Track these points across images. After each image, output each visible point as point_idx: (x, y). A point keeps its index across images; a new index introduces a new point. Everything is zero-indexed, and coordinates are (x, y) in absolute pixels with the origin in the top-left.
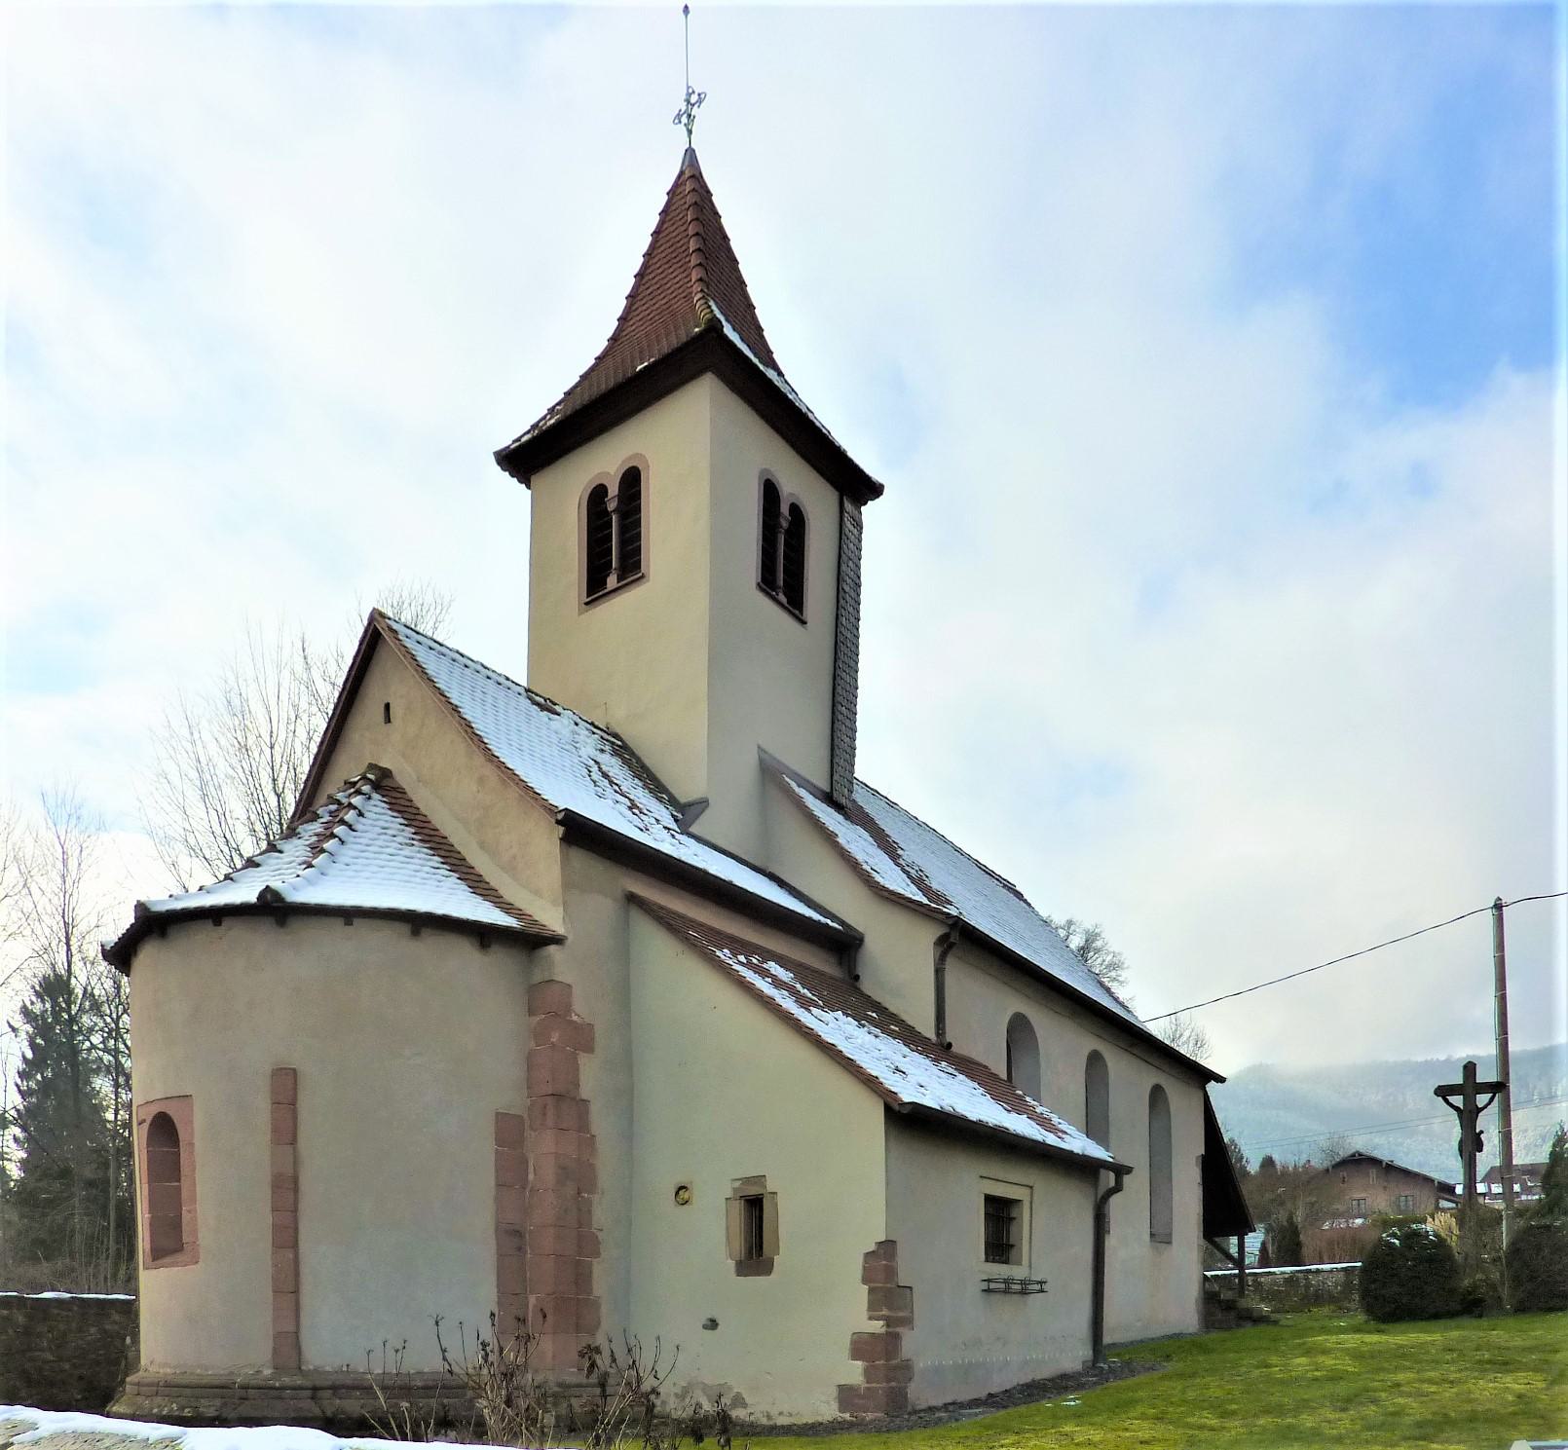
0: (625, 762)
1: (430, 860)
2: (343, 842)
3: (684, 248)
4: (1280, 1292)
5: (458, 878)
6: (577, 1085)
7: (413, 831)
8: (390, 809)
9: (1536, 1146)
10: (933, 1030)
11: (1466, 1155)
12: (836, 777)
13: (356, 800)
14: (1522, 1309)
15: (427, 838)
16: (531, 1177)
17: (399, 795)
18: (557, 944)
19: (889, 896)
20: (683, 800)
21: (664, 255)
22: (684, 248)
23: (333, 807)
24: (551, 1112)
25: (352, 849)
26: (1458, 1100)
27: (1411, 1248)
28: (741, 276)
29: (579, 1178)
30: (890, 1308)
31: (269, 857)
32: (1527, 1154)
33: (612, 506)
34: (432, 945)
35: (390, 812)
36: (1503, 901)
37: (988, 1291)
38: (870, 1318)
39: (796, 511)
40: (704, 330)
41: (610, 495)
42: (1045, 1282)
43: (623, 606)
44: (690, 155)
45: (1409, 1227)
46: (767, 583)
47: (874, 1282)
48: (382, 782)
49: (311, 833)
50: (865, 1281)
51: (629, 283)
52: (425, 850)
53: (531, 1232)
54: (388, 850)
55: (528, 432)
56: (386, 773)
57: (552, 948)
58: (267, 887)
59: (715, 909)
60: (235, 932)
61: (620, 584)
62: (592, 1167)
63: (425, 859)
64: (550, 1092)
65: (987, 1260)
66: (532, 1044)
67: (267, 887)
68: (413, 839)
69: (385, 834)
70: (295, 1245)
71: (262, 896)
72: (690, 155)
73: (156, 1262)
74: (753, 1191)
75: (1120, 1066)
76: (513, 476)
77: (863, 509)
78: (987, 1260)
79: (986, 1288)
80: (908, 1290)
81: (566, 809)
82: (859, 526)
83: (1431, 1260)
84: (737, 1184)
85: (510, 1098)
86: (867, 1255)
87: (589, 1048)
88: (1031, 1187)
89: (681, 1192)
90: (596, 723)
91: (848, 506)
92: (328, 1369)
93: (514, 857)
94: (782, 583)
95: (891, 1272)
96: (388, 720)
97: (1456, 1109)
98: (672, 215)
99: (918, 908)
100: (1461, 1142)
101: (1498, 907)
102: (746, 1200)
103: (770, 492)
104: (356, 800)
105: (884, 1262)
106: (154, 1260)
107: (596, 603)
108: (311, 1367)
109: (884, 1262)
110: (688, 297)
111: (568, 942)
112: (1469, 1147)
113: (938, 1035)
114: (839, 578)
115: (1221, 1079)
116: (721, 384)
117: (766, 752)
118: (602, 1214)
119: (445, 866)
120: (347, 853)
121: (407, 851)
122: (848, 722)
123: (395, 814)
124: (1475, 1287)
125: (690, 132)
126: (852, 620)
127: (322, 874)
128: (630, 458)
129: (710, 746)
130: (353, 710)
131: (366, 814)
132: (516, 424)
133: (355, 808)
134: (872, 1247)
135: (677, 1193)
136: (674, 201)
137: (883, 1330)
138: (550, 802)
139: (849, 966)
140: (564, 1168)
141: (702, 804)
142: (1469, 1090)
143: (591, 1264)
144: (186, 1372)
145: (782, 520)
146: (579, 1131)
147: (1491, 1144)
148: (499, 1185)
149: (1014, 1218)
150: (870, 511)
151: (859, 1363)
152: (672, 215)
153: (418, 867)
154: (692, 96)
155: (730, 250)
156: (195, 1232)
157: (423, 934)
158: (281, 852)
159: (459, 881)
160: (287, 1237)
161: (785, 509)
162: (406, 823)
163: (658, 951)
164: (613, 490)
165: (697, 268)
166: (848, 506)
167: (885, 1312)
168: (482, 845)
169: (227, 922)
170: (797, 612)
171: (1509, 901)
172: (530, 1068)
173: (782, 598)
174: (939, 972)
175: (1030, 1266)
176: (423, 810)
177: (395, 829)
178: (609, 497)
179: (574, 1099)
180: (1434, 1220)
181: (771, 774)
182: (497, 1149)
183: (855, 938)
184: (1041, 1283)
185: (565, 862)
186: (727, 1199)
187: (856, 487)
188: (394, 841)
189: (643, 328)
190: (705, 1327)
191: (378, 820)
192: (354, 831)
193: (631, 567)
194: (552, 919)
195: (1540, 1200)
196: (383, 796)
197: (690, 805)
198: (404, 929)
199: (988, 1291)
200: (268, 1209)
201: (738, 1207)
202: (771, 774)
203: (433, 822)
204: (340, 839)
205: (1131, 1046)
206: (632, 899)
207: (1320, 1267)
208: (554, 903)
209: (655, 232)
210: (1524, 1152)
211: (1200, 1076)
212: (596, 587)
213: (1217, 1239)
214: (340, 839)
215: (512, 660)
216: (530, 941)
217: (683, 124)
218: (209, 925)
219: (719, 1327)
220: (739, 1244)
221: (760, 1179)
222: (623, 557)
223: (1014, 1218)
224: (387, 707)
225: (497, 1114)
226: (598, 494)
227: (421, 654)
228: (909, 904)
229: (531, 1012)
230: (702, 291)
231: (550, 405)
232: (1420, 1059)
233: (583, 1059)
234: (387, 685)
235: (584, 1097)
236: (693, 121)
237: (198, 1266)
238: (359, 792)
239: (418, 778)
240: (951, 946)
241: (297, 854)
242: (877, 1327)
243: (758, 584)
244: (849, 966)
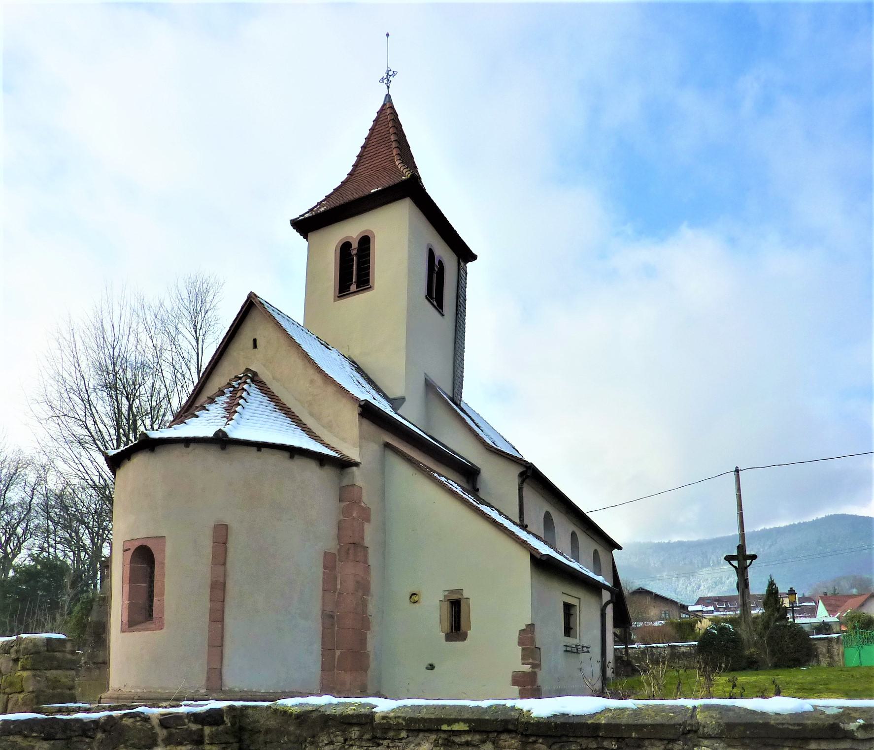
0: (362, 375)
1: (286, 420)
2: (244, 408)
3: (388, 138)
4: (638, 657)
5: (301, 430)
6: (363, 539)
7: (274, 404)
8: (261, 392)
9: (712, 587)
10: (518, 518)
11: (741, 589)
12: (456, 390)
13: (245, 387)
14: (777, 666)
15: (282, 408)
16: (339, 587)
17: (263, 385)
19: (495, 451)
20: (391, 396)
21: (376, 140)
22: (388, 138)
23: (231, 389)
24: (351, 551)
25: (248, 412)
26: (735, 563)
27: (723, 635)
28: (411, 154)
29: (363, 587)
30: (533, 659)
31: (203, 413)
32: (709, 591)
33: (354, 252)
34: (299, 463)
35: (260, 393)
36: (739, 469)
37: (566, 651)
38: (523, 664)
39: (440, 262)
40: (408, 179)
41: (353, 247)
42: (565, 651)
43: (358, 301)
44: (388, 96)
45: (721, 625)
46: (429, 296)
47: (524, 645)
48: (255, 378)
49: (223, 401)
50: (520, 644)
51: (358, 151)
52: (282, 414)
53: (337, 616)
54: (266, 413)
55: (308, 212)
56: (255, 374)
57: (354, 468)
58: (220, 429)
59: (420, 453)
60: (196, 451)
61: (358, 290)
62: (368, 582)
63: (283, 419)
64: (352, 542)
65: (565, 636)
66: (342, 517)
67: (220, 429)
68: (275, 408)
69: (262, 405)
70: (222, 620)
71: (216, 434)
72: (388, 96)
73: (130, 629)
74: (455, 597)
76: (301, 235)
77: (467, 265)
78: (565, 636)
79: (565, 650)
80: (538, 649)
81: (366, 400)
82: (466, 273)
83: (733, 641)
84: (446, 593)
85: (331, 545)
86: (521, 631)
87: (368, 520)
89: (413, 597)
90: (345, 355)
91: (462, 263)
92: (237, 689)
94: (435, 297)
95: (532, 640)
96: (255, 346)
97: (735, 567)
98: (380, 123)
99: (510, 457)
100: (738, 584)
101: (737, 471)
102: (451, 602)
103: (431, 254)
104: (245, 387)
105: (530, 635)
106: (129, 627)
107: (345, 297)
108: (227, 689)
109: (530, 635)
110: (393, 161)
111: (361, 466)
112: (742, 586)
113: (520, 520)
115: (620, 548)
116: (397, 202)
117: (428, 376)
118: (372, 608)
119: (293, 423)
120: (247, 414)
121: (274, 414)
123: (264, 395)
124: (752, 654)
125: (388, 87)
126: (463, 315)
127: (238, 424)
129: (406, 373)
130: (233, 340)
131: (251, 394)
132: (302, 207)
133: (246, 390)
134: (524, 627)
135: (411, 597)
136: (381, 116)
137: (531, 670)
138: (355, 395)
139: (473, 484)
140: (357, 582)
141: (402, 400)
142: (741, 558)
143: (366, 633)
144: (151, 691)
145: (435, 268)
146: (364, 564)
147: (691, 586)
148: (324, 590)
149: (572, 614)
151: (517, 687)
152: (380, 123)
153: (282, 423)
154: (390, 72)
155: (406, 141)
156: (162, 611)
157: (295, 459)
158: (208, 410)
159: (302, 431)
160: (217, 617)
161: (437, 263)
162: (270, 400)
163: (401, 472)
164: (355, 245)
165: (397, 149)
166: (462, 263)
167: (531, 661)
168: (311, 414)
169: (192, 446)
170: (441, 310)
171: (742, 469)
172: (339, 529)
173: (435, 303)
174: (520, 490)
175: (580, 639)
176: (276, 393)
177: (266, 403)
178: (353, 248)
179: (362, 546)
180: (701, 623)
181: (430, 386)
182: (324, 571)
183: (477, 470)
184: (588, 647)
185: (360, 424)
186: (440, 601)
187: (465, 255)
188: (267, 409)
189: (367, 171)
190: (427, 668)
191: (257, 397)
192: (247, 402)
193: (364, 282)
194: (353, 454)
195: (763, 613)
196: (256, 385)
197: (395, 399)
198: (287, 454)
199: (566, 651)
200: (208, 600)
201: (447, 606)
202: (430, 386)
203: (282, 400)
204: (242, 406)
205: (587, 529)
206: (387, 445)
207: (658, 645)
208: (354, 446)
209: (371, 129)
210: (707, 590)
211: (612, 545)
212: (344, 289)
214: (242, 406)
215: (299, 318)
216: (343, 464)
217: (385, 83)
218: (182, 445)
219: (435, 668)
220: (447, 625)
221: (460, 591)
223: (572, 614)
224: (255, 341)
225: (325, 553)
226: (345, 247)
227: (278, 318)
228: (506, 455)
229: (341, 500)
230: (400, 159)
231: (319, 201)
232: (656, 541)
234: (254, 328)
235: (366, 545)
236: (390, 82)
237: (163, 631)
238: (245, 383)
239: (273, 377)
240: (528, 477)
241: (218, 412)
242: (527, 668)
243: (426, 296)
244: (473, 484)
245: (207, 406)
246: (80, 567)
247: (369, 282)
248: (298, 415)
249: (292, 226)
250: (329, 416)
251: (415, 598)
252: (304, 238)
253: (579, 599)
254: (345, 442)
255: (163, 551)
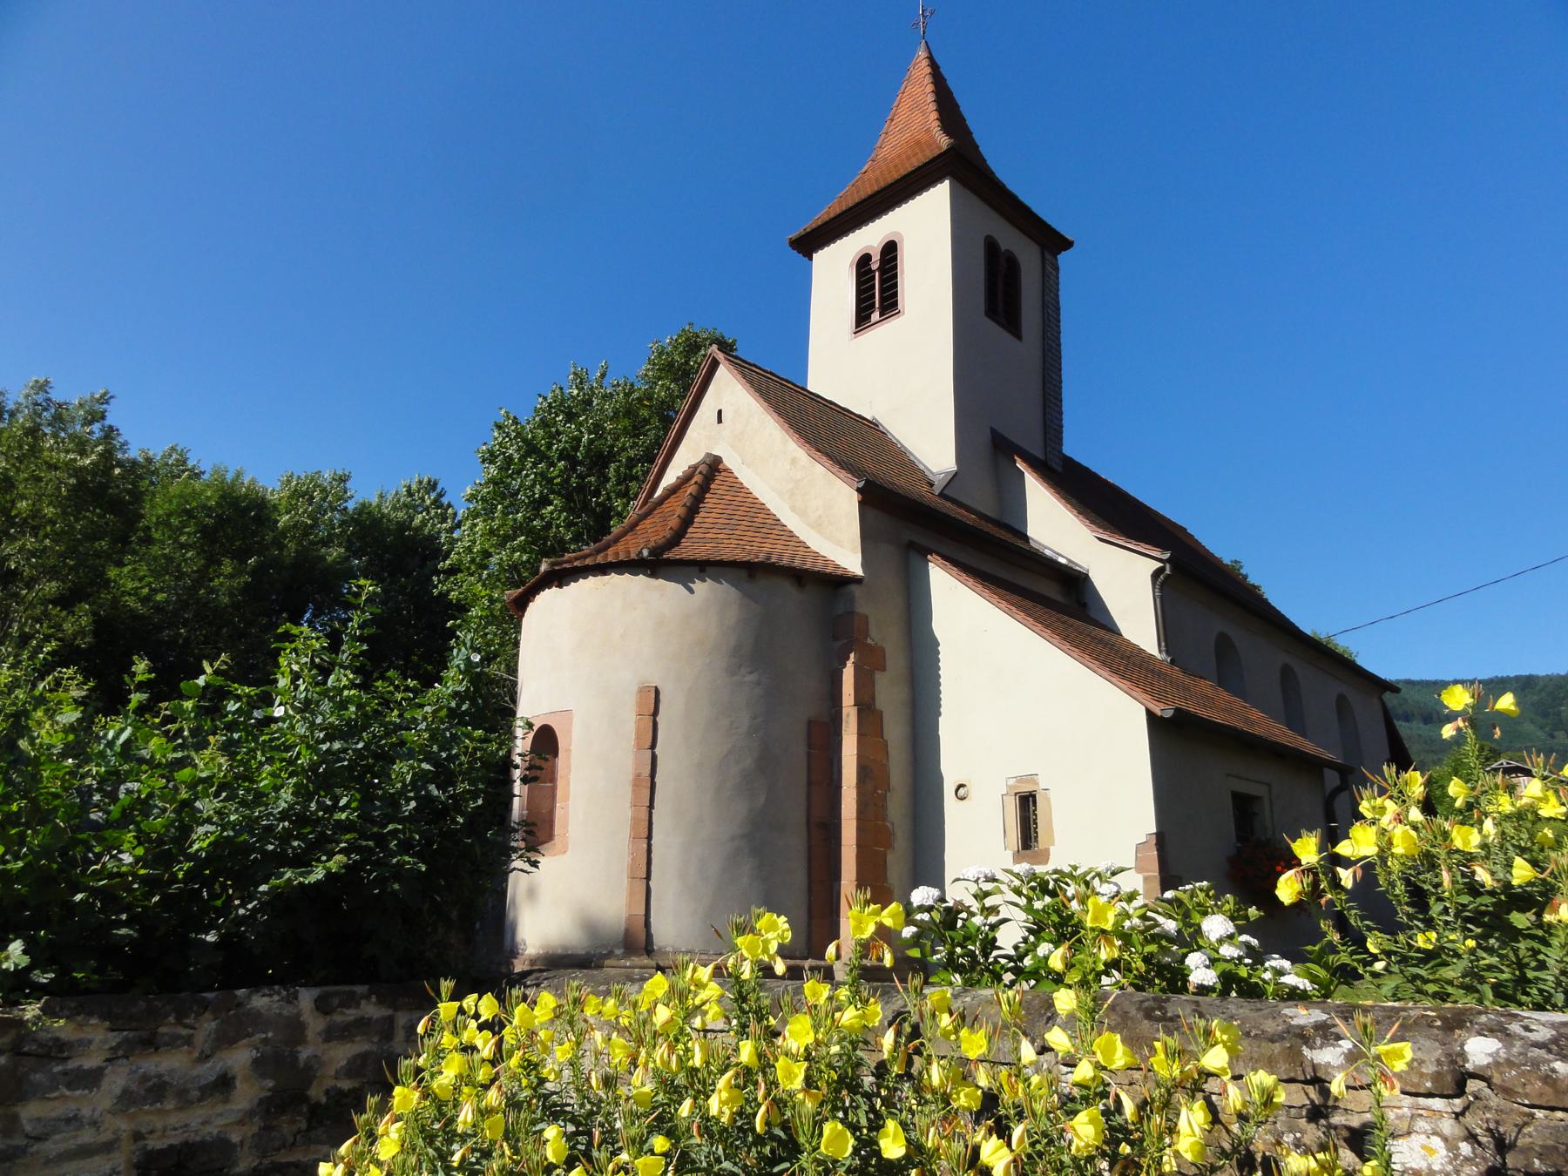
18: (1392, 692)
33: (875, 266)
43: (884, 332)
46: (991, 312)
74: (1026, 788)
75: (1305, 673)
82: (1057, 269)
84: (1012, 782)
88: (1269, 785)
93: (820, 517)
96: (720, 420)
103: (991, 246)
111: (864, 582)
114: (1044, 306)
122: (1056, 408)
128: (868, 247)
150: (1064, 258)
164: (876, 257)
166: (1048, 256)
168: (793, 509)
176: (745, 485)
187: (1053, 243)
193: (890, 305)
198: (743, 573)
212: (862, 319)
213: (691, 585)
221: (1032, 778)
222: (882, 300)
226: (864, 261)
233: (878, 675)
245: (179, 452)
246: (346, 763)
247: (897, 305)
248: (774, 512)
249: (793, 249)
250: (817, 509)
251: (962, 792)
252: (804, 256)
253: (1269, 785)
254: (842, 547)
255: (569, 732)
